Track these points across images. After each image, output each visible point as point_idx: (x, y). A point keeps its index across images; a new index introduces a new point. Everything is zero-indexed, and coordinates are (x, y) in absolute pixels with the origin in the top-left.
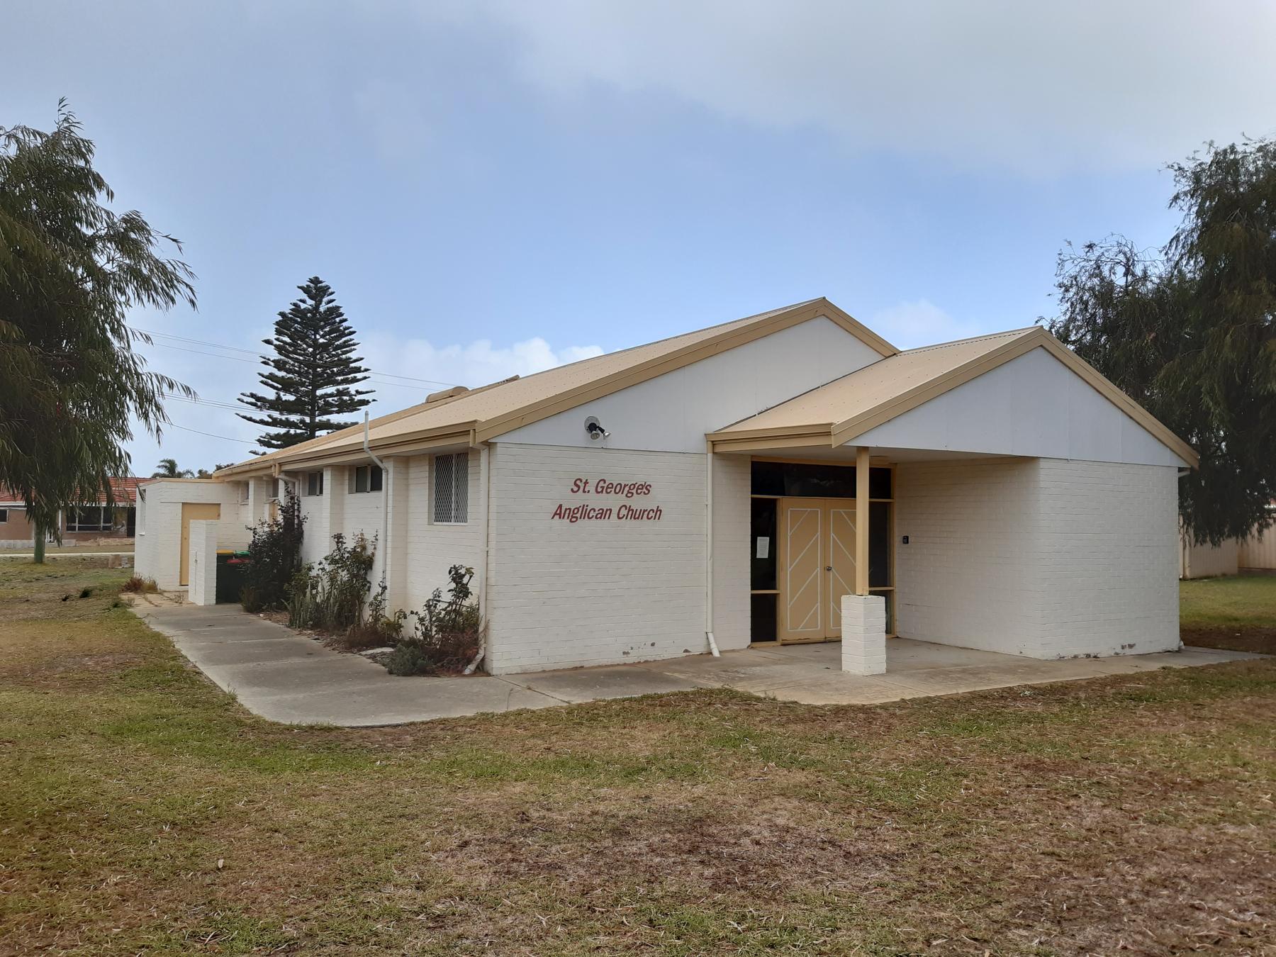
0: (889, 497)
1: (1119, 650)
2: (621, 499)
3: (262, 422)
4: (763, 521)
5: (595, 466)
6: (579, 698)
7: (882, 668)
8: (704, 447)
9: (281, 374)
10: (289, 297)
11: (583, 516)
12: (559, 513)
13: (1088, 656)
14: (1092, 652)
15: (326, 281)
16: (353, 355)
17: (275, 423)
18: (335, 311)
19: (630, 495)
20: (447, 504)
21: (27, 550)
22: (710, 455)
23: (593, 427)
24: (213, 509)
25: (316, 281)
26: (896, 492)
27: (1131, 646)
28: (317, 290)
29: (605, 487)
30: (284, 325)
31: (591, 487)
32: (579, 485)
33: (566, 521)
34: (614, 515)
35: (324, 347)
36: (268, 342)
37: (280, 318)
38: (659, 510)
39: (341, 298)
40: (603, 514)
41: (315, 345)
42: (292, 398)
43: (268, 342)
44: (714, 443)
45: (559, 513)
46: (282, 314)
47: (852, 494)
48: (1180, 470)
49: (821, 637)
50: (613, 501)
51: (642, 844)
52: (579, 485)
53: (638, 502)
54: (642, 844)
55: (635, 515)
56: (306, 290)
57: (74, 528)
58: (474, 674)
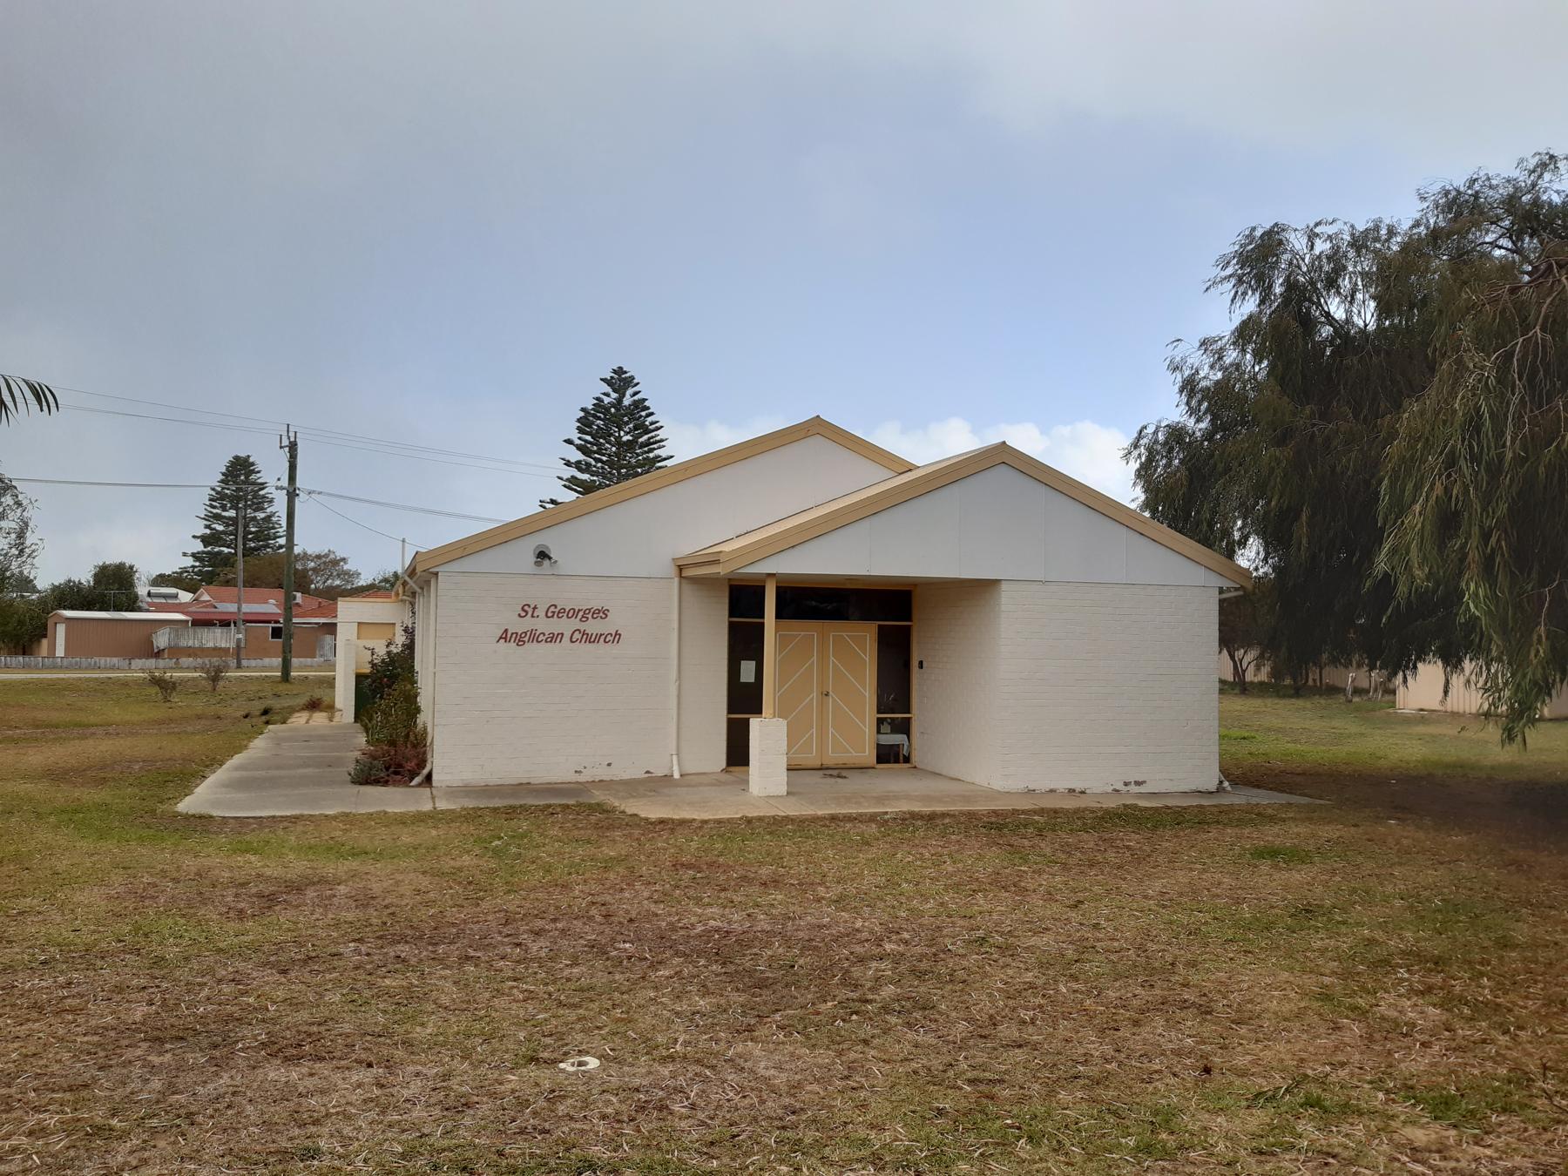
0: (910, 619)
1: (1120, 786)
2: (575, 623)
4: (744, 642)
5: (544, 592)
6: (470, 803)
7: (783, 790)
8: (673, 572)
9: (585, 477)
10: (591, 391)
12: (505, 636)
13: (1072, 791)
14: (1078, 786)
15: (631, 370)
16: (662, 453)
18: (640, 405)
19: (584, 619)
21: (271, 669)
22: (676, 580)
23: (543, 555)
25: (619, 371)
26: (915, 614)
27: (1138, 783)
28: (620, 381)
29: (555, 612)
30: (585, 423)
31: (541, 612)
32: (527, 610)
33: (513, 644)
34: (566, 639)
35: (631, 445)
36: (569, 442)
39: (649, 389)
40: (553, 638)
41: (619, 443)
43: (569, 442)
44: (680, 568)
45: (505, 636)
46: (583, 410)
48: (1221, 591)
49: (817, 764)
50: (566, 626)
52: (527, 610)
53: (593, 626)
55: (588, 638)
58: (419, 785)
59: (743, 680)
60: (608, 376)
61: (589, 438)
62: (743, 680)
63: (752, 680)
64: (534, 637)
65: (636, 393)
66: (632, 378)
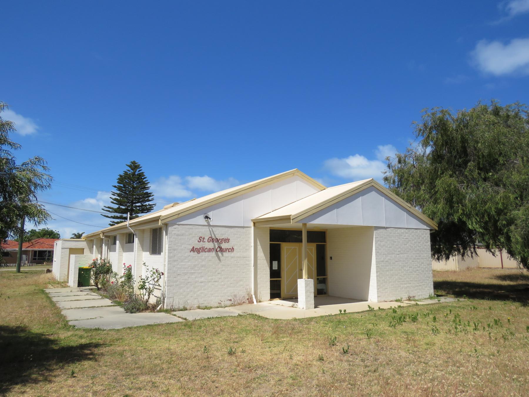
0: (325, 242)
3: (112, 217)
4: (275, 254)
10: (123, 169)
11: (202, 251)
12: (193, 250)
15: (139, 162)
17: (114, 217)
18: (141, 175)
20: (155, 248)
24: (81, 251)
25: (134, 163)
28: (134, 166)
30: (121, 180)
31: (206, 240)
32: (201, 239)
33: (196, 253)
37: (119, 177)
38: (233, 249)
39: (146, 170)
42: (123, 207)
43: (115, 187)
45: (193, 250)
47: (301, 241)
51: (522, 335)
52: (201, 239)
54: (522, 335)
56: (130, 166)
57: (35, 259)
59: (277, 262)
60: (129, 164)
61: (122, 185)
62: (277, 262)
63: (273, 262)
64: (203, 250)
65: (140, 171)
66: (139, 165)
